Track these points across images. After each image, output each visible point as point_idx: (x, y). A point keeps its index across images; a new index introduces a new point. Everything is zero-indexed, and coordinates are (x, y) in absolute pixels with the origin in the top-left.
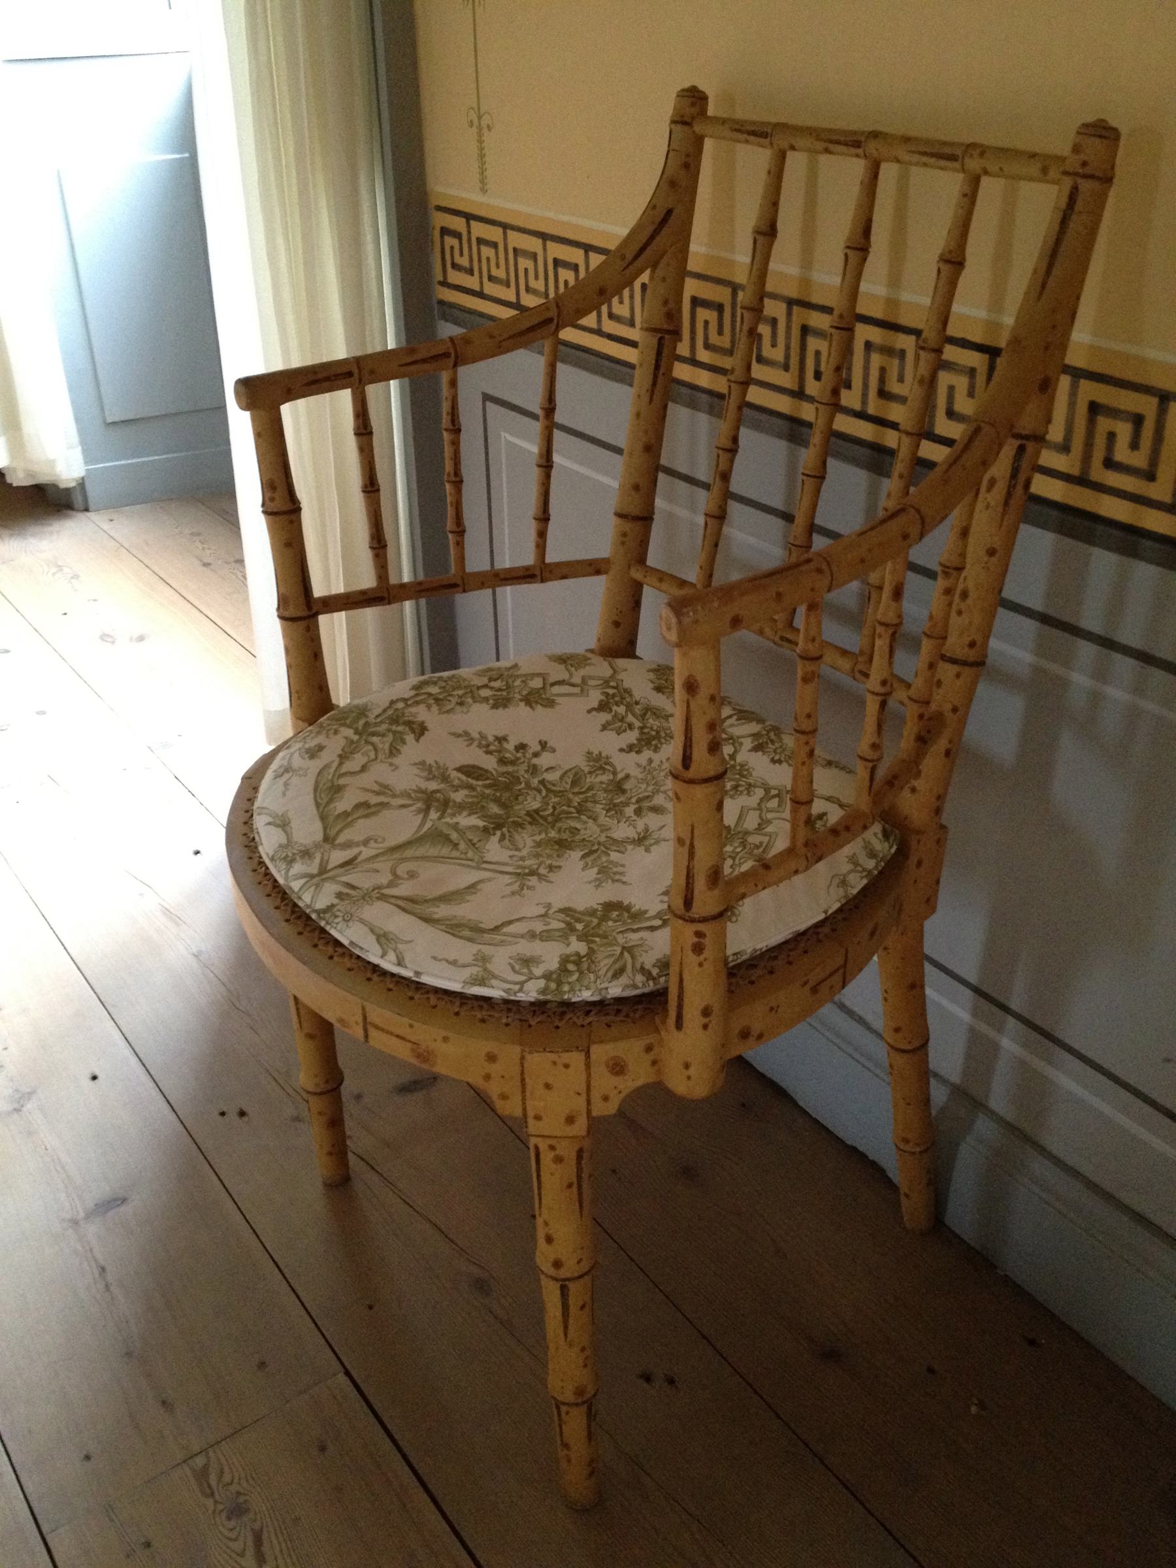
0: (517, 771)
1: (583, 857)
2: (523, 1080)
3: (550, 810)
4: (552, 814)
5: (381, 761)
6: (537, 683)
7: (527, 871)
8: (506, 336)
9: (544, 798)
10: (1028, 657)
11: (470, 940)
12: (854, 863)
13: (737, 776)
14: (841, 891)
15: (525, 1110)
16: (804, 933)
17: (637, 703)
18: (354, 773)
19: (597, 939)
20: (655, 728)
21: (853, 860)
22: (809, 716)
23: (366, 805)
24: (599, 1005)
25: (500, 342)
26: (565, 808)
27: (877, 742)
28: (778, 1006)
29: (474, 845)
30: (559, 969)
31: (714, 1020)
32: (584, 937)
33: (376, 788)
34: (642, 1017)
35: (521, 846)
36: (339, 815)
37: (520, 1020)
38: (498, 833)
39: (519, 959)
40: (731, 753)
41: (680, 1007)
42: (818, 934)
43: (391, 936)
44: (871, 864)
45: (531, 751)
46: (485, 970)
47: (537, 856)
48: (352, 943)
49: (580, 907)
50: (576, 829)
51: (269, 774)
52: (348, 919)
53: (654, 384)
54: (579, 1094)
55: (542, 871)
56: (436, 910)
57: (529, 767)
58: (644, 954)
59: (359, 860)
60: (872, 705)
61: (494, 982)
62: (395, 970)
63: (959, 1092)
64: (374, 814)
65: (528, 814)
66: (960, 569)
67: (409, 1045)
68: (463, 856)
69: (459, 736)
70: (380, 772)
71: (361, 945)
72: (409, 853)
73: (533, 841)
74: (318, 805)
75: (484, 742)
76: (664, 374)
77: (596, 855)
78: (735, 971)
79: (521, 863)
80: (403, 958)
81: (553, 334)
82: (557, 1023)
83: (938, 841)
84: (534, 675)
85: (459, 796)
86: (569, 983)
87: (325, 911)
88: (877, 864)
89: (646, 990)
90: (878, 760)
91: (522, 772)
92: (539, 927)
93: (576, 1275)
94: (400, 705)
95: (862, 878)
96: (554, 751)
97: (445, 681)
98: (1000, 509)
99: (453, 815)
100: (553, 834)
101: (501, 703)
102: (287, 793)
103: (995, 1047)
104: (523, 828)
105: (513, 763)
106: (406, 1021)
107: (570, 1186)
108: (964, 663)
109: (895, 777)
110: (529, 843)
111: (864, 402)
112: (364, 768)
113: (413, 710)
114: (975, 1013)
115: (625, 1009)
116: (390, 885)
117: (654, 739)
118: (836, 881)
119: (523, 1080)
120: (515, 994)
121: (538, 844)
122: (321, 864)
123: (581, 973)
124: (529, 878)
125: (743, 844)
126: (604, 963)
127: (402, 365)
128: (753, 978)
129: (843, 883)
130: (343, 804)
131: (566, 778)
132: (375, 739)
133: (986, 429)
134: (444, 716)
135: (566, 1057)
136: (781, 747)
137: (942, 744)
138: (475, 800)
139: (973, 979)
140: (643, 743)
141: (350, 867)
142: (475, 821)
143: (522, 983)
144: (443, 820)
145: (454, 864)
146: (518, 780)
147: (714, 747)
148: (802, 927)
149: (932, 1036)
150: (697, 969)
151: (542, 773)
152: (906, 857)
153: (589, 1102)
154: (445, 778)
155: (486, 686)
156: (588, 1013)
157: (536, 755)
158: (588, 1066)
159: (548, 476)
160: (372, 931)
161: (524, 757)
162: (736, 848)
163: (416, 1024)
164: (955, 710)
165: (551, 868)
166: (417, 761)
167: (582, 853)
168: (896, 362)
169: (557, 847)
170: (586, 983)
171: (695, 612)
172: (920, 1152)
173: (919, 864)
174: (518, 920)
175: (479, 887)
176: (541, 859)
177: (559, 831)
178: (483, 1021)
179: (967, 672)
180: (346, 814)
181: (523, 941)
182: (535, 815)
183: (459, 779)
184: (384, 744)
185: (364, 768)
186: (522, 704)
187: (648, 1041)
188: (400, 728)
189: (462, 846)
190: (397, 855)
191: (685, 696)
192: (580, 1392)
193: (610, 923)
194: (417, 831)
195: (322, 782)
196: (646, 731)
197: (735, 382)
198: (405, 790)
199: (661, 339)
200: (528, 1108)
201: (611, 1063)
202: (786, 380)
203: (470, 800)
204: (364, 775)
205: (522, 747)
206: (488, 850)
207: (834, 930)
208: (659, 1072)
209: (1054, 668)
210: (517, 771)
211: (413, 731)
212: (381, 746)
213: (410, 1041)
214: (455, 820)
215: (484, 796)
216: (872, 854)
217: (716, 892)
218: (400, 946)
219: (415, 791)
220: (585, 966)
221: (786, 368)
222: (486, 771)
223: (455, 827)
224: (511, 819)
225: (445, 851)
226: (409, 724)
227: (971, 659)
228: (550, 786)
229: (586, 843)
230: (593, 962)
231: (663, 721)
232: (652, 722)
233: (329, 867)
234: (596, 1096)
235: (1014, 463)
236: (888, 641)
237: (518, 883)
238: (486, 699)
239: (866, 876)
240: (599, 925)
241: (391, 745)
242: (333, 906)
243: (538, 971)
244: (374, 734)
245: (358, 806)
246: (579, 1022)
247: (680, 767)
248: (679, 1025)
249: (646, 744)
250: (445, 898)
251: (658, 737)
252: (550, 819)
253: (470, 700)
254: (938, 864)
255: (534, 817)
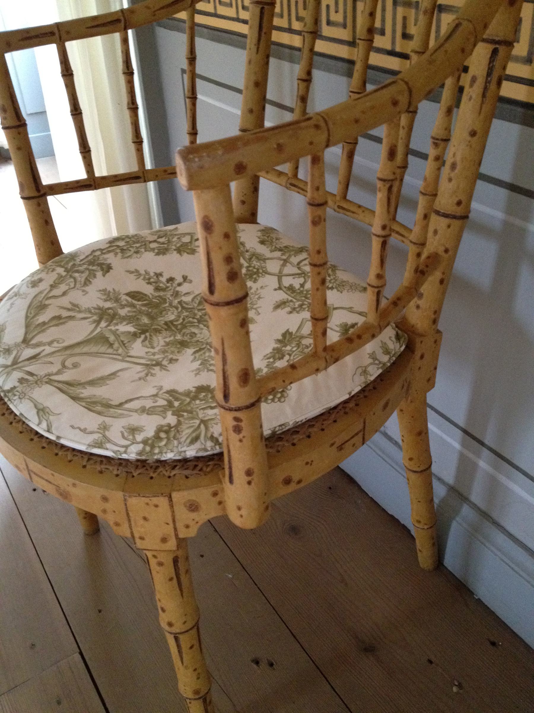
0: (165, 295)
1: (195, 353)
2: (128, 514)
3: (181, 321)
4: (182, 324)
5: (78, 289)
6: (187, 239)
7: (154, 362)
8: (157, 7)
9: (179, 313)
10: (499, 215)
11: (99, 413)
12: (373, 359)
13: (303, 298)
14: (363, 379)
15: (132, 533)
16: (335, 408)
17: (247, 251)
18: (57, 296)
19: (185, 414)
20: (257, 267)
21: (373, 356)
22: (319, 252)
23: (59, 317)
24: (184, 462)
25: (154, 12)
26: (191, 319)
27: (381, 273)
28: (312, 461)
29: (124, 344)
30: (154, 436)
31: (255, 478)
32: (177, 413)
33: (70, 306)
34: (212, 470)
35: (155, 345)
36: (39, 325)
37: (127, 472)
38: (143, 336)
39: (129, 429)
40: (302, 283)
41: (230, 468)
42: (344, 408)
43: (47, 410)
44: (385, 359)
45: (176, 282)
46: (104, 436)
47: (164, 352)
48: (21, 414)
49: (181, 389)
50: (194, 333)
51: (6, 298)
52: (23, 396)
53: (259, 40)
54: (168, 524)
55: (165, 363)
56: (83, 391)
57: (173, 292)
58: (215, 426)
59: (42, 355)
60: (376, 244)
61: (108, 445)
62: (46, 434)
63: (452, 489)
64: (63, 323)
65: (166, 323)
66: (447, 140)
67: (54, 487)
68: (115, 352)
69: (131, 272)
70: (76, 296)
71: (26, 416)
72: (77, 350)
73: (165, 342)
74: (27, 317)
75: (147, 277)
76: (265, 33)
77: (203, 351)
78: (283, 436)
79: (152, 357)
80: (51, 426)
81: (190, 6)
82: (152, 474)
83: (435, 342)
84: (185, 234)
85: (123, 312)
86: (159, 447)
87: (9, 391)
88: (390, 359)
89: (215, 452)
90: (382, 287)
91: (169, 296)
92: (149, 403)
93: (183, 631)
94: (98, 253)
95: (378, 369)
96: (191, 282)
97: (130, 238)
98: (480, 99)
99: (117, 324)
100: (179, 337)
101: (162, 251)
102: (11, 311)
103: (475, 466)
104: (160, 333)
105: (164, 290)
106: (49, 472)
107: (171, 579)
108: (454, 217)
109: (399, 299)
110: (162, 343)
111: (393, 43)
112: (64, 294)
113: (106, 256)
114: (463, 444)
115: (200, 465)
116: (58, 373)
117: (255, 274)
118: (360, 370)
119: (128, 514)
120: (121, 454)
121: (167, 344)
122: (15, 358)
123: (168, 439)
124: (154, 367)
125: (298, 345)
126: (186, 432)
127: (88, 28)
128: (295, 441)
129: (365, 372)
130: (43, 317)
131: (195, 300)
132: (76, 275)
133: (465, 23)
134: (126, 260)
135: (155, 500)
136: (334, 278)
137: (437, 275)
138: (134, 314)
139: (461, 423)
140: (248, 277)
141: (34, 360)
142: (130, 328)
143: (127, 447)
144: (109, 328)
145: (106, 358)
146: (165, 301)
147: (233, 276)
148: (333, 404)
149: (433, 459)
150: (238, 443)
151: (182, 296)
152: (413, 352)
153: (175, 529)
154: (117, 300)
155: (155, 241)
156: (174, 468)
157: (180, 285)
158: (172, 506)
159: (194, 104)
160: (36, 406)
161: (172, 286)
162: (293, 348)
163: (56, 474)
164: (446, 251)
165: (171, 361)
166: (101, 289)
167: (193, 350)
168: (413, 11)
169: (179, 346)
170: (170, 447)
171: (201, 158)
172: (428, 529)
173: (422, 357)
174: (138, 398)
175: (118, 374)
176: (166, 354)
177: (184, 335)
178: (101, 472)
179: (456, 223)
180: (44, 323)
181: (134, 414)
182: (170, 324)
183: (127, 300)
184: (81, 278)
185: (64, 294)
186: (175, 252)
187: (213, 489)
188: (94, 268)
189: (116, 345)
190: (68, 352)
191: (205, 234)
192: (196, 692)
193: (198, 402)
194: (89, 335)
195: (35, 303)
196: (251, 269)
197: (307, 32)
198: (88, 308)
199: (262, 8)
200: (134, 532)
201: (188, 505)
202: (344, 34)
203: (131, 314)
204: (64, 298)
205: (171, 280)
206: (133, 348)
207: (357, 405)
208: (224, 509)
209: (518, 222)
210: (165, 295)
211: (102, 269)
212: (79, 279)
213: (54, 484)
214: (117, 327)
215: (140, 312)
216: (387, 352)
217: (247, 389)
218: (51, 418)
219: (95, 308)
220: (172, 434)
221: (345, 26)
222: (146, 295)
223: (115, 333)
224: (153, 327)
225: (103, 349)
226: (101, 265)
227: (458, 214)
228: (184, 305)
229: (198, 343)
230: (178, 431)
231: (262, 262)
232: (255, 263)
233: (20, 360)
234: (180, 526)
235: (489, 64)
236: (386, 193)
237: (146, 371)
238: (153, 250)
239: (381, 368)
240: (189, 403)
241: (86, 279)
242: (15, 387)
243: (139, 438)
244: (77, 271)
245: (54, 318)
246: (167, 474)
247: (207, 292)
248: (231, 481)
249: (250, 277)
250: (92, 383)
251: (257, 273)
252: (179, 327)
253: (143, 250)
254: (436, 358)
255: (169, 325)
